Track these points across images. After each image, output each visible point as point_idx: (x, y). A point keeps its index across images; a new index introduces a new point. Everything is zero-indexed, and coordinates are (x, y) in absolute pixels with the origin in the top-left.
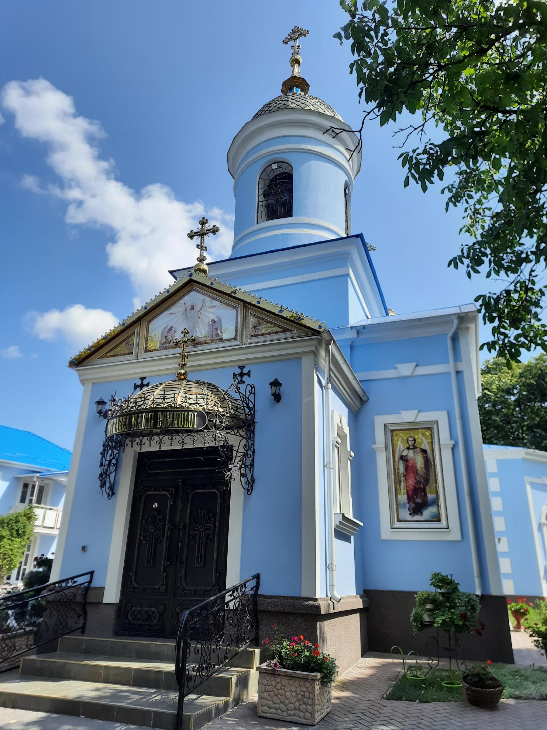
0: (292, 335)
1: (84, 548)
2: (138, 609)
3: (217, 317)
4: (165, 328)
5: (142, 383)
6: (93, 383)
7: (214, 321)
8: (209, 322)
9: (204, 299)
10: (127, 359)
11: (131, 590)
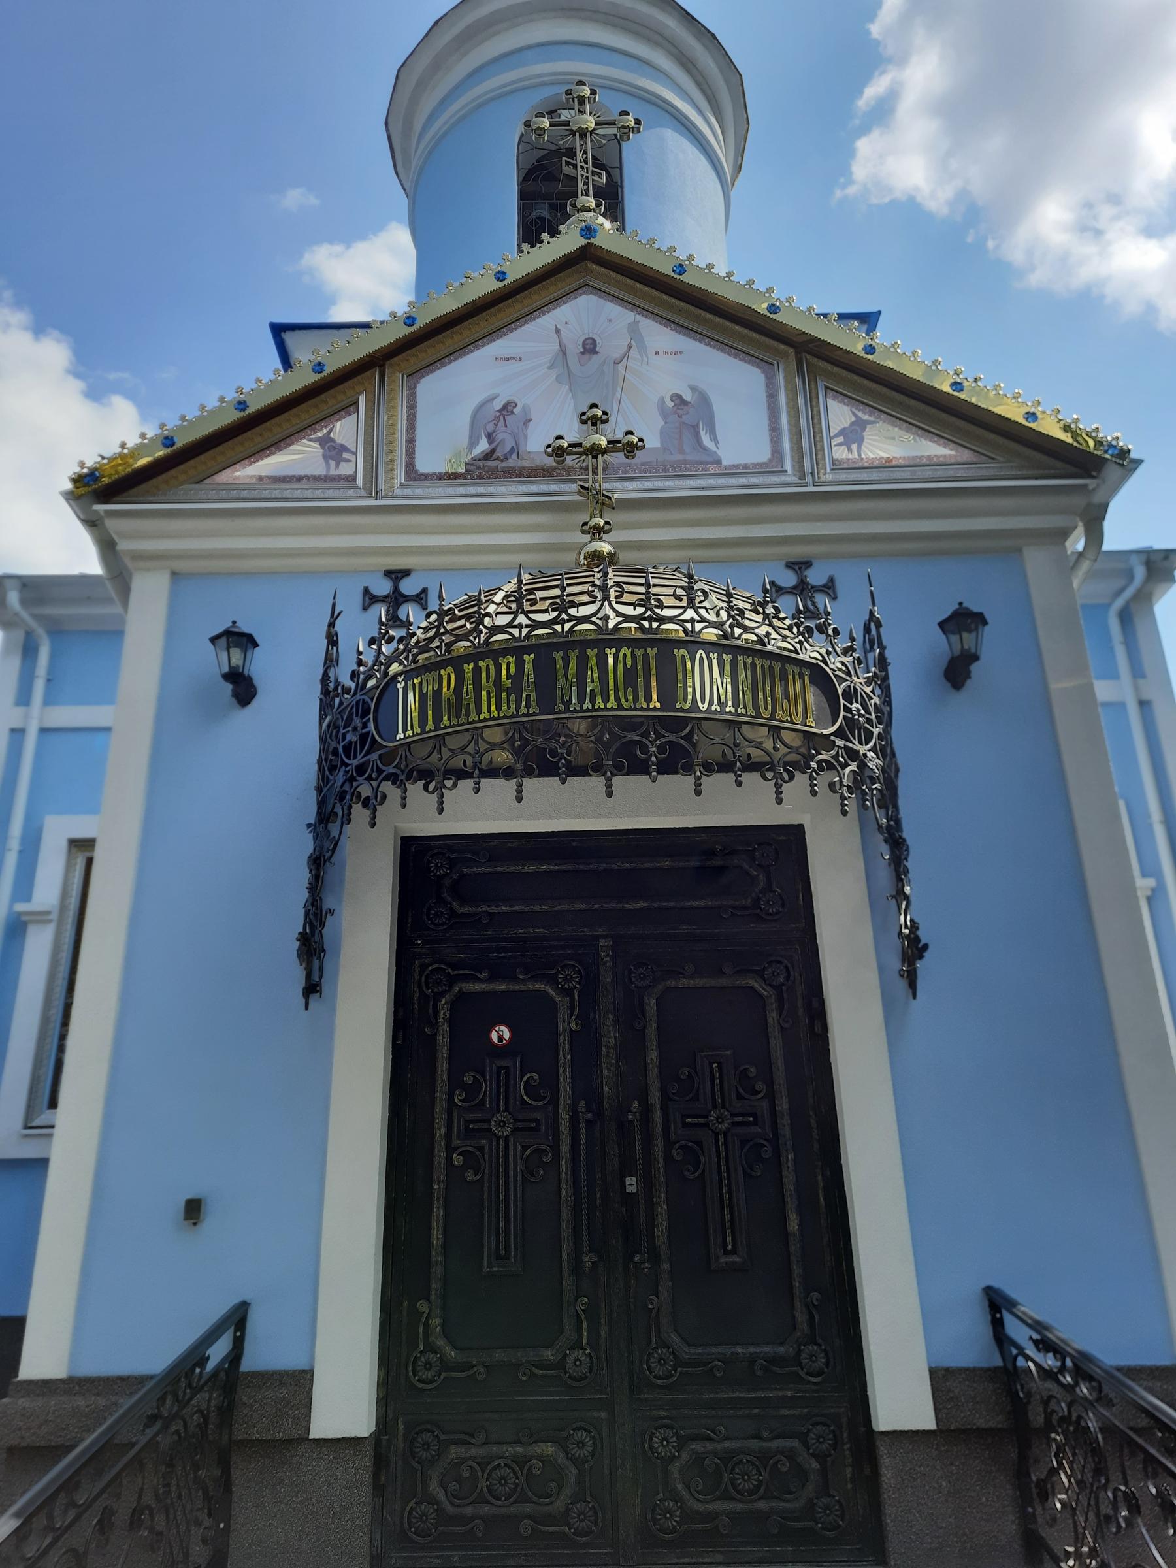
0: (992, 473)
1: (193, 1210)
2: (473, 1452)
3: (693, 389)
4: (481, 406)
5: (396, 590)
6: (174, 574)
7: (678, 399)
8: (662, 400)
9: (636, 323)
10: (330, 493)
11: (429, 1375)
